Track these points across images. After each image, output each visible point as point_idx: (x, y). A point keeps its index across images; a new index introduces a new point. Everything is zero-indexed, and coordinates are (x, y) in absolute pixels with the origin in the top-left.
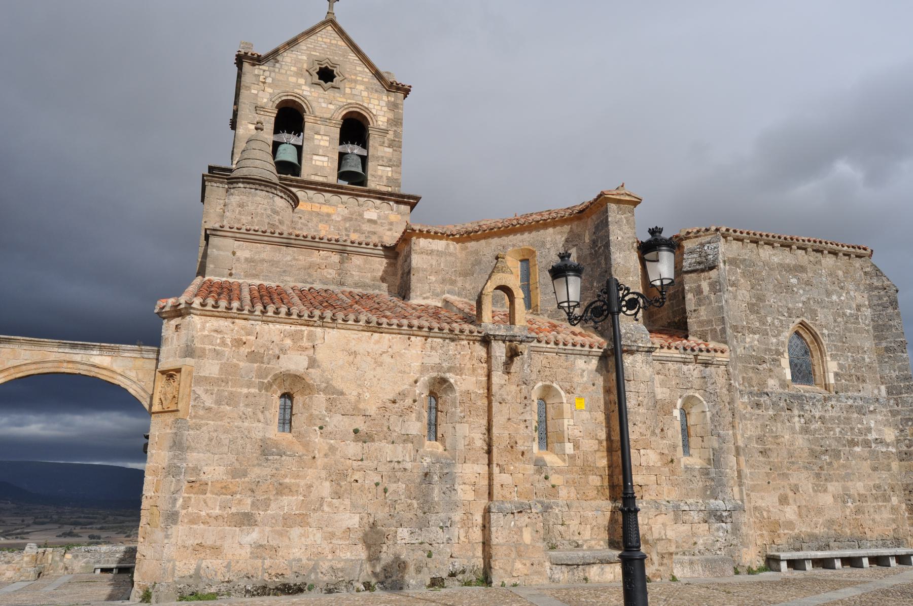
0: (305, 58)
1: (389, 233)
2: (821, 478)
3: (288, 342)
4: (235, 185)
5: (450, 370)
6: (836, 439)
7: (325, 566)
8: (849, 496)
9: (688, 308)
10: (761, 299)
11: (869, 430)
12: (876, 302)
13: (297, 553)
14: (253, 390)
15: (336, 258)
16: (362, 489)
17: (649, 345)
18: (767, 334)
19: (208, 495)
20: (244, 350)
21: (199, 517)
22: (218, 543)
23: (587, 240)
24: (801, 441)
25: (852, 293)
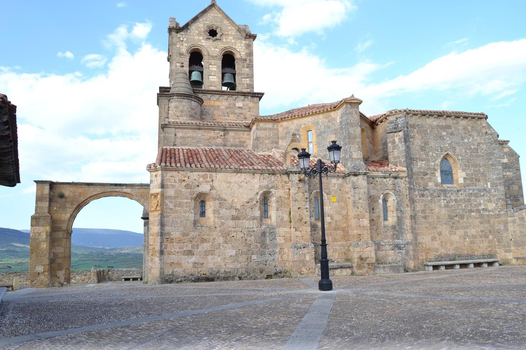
0: (202, 25)
1: (249, 113)
2: (453, 228)
3: (201, 179)
4: (172, 98)
5: (272, 188)
6: (462, 209)
7: (222, 271)
8: (468, 236)
9: (389, 151)
10: (426, 143)
11: (480, 204)
12: (487, 141)
13: (211, 266)
14: (188, 201)
15: (222, 133)
16: (236, 240)
17: (365, 171)
18: (429, 161)
19: (174, 243)
20: (184, 184)
21: (172, 252)
22: (180, 262)
23: (338, 121)
24: (444, 211)
25: (475, 137)
